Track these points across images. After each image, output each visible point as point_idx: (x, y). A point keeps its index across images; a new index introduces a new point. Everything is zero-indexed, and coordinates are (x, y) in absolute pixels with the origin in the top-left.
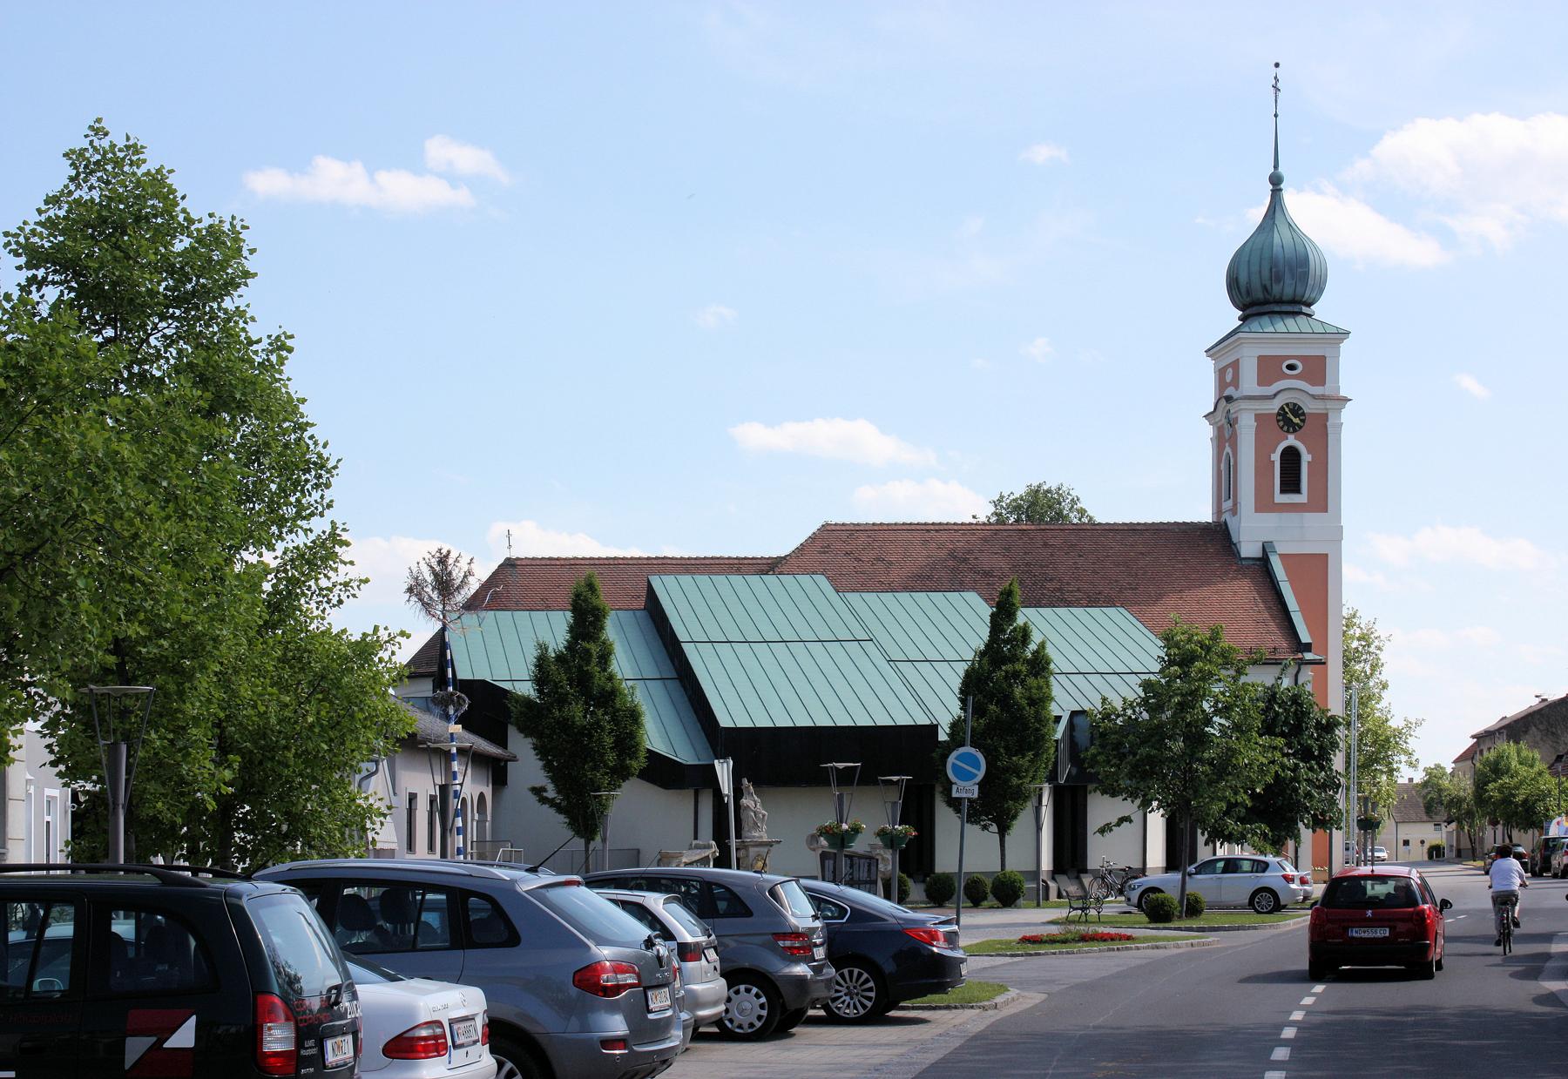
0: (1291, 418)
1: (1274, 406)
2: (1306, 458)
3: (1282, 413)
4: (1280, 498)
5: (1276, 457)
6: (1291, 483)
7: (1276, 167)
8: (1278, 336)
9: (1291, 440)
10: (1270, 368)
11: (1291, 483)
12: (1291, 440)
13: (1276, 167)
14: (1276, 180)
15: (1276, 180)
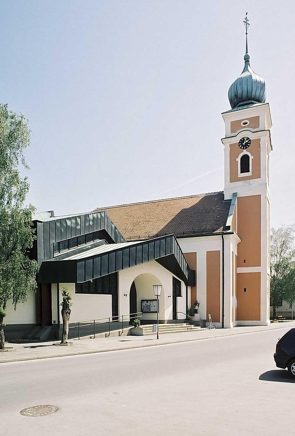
0: (244, 144)
1: (237, 140)
2: (251, 158)
3: (242, 141)
4: (241, 175)
5: (239, 160)
6: (245, 168)
8: (245, 114)
9: (245, 152)
10: (235, 126)
11: (245, 168)
12: (245, 152)
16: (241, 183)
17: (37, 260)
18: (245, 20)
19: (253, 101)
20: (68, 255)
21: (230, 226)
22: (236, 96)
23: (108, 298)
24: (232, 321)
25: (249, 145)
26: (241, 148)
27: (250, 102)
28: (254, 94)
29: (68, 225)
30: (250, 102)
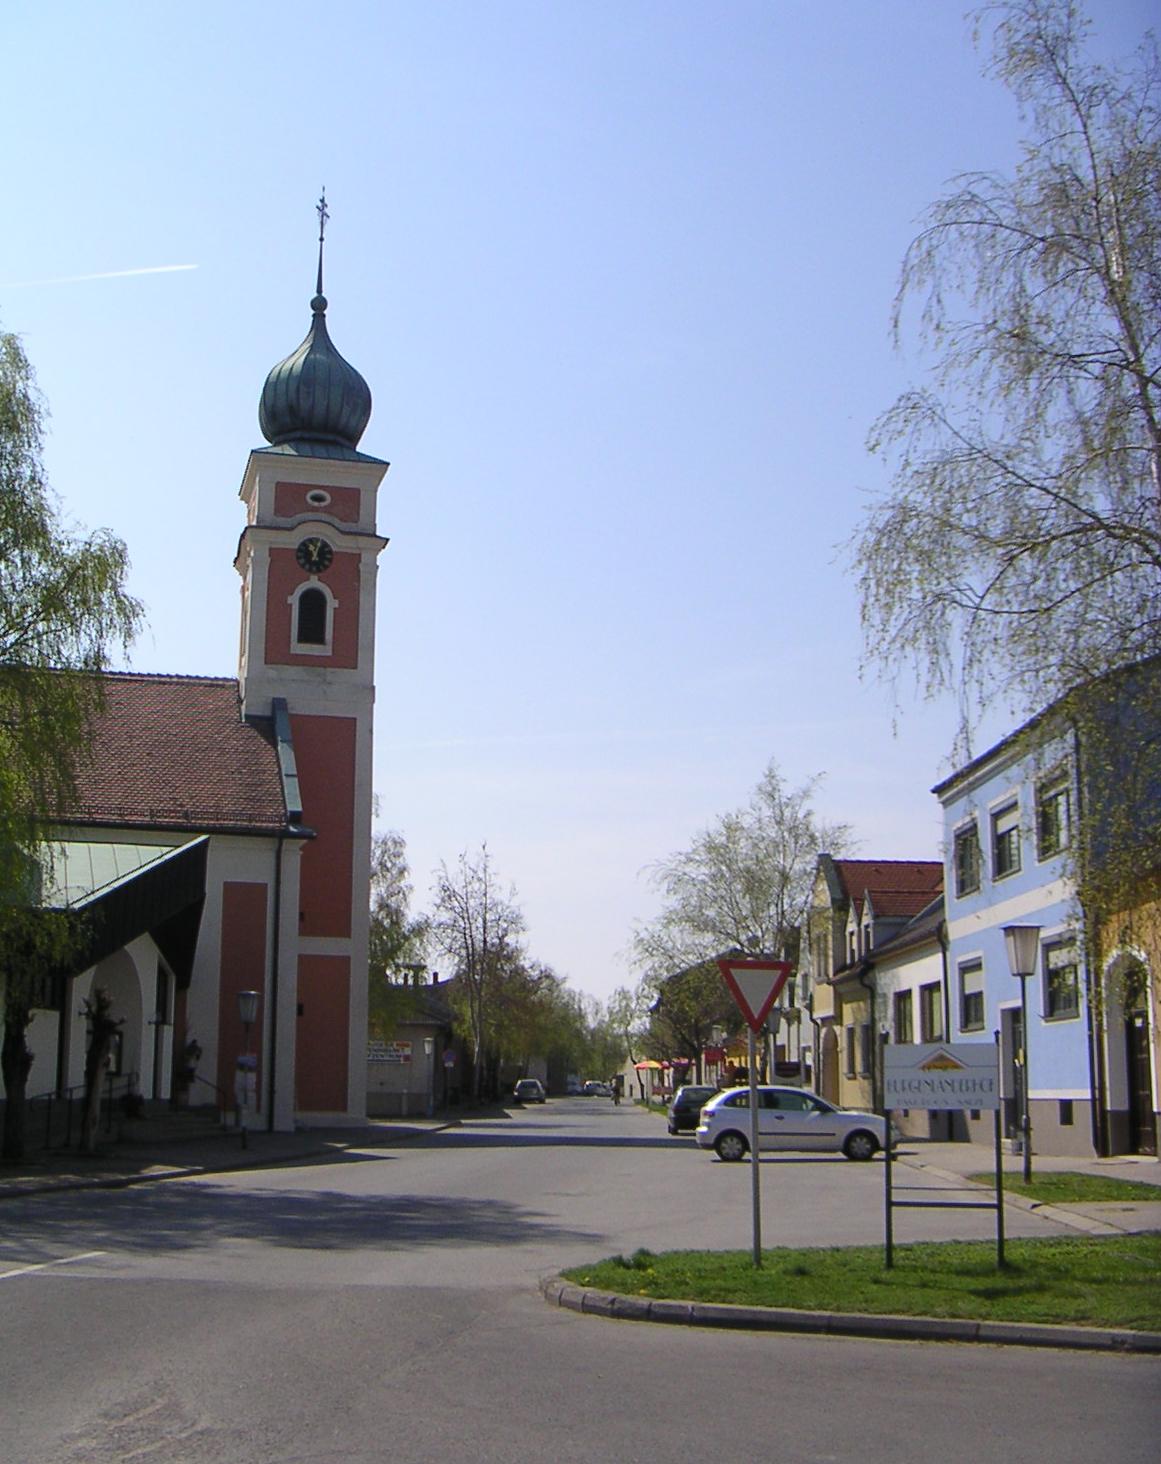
2: (332, 604)
3: (304, 550)
4: (299, 648)
5: (294, 600)
6: (311, 630)
7: (319, 290)
9: (314, 582)
11: (311, 630)
12: (314, 582)
13: (319, 290)
14: (319, 305)
15: (319, 305)
16: (292, 672)
17: (841, 1025)
18: (320, 204)
19: (340, 439)
20: (42, 1270)
21: (344, 1108)
22: (292, 410)
23: (925, 1135)
24: (958, 1026)
25: (307, 566)
27: (331, 437)
28: (343, 420)
29: (293, 1130)
30: (331, 437)
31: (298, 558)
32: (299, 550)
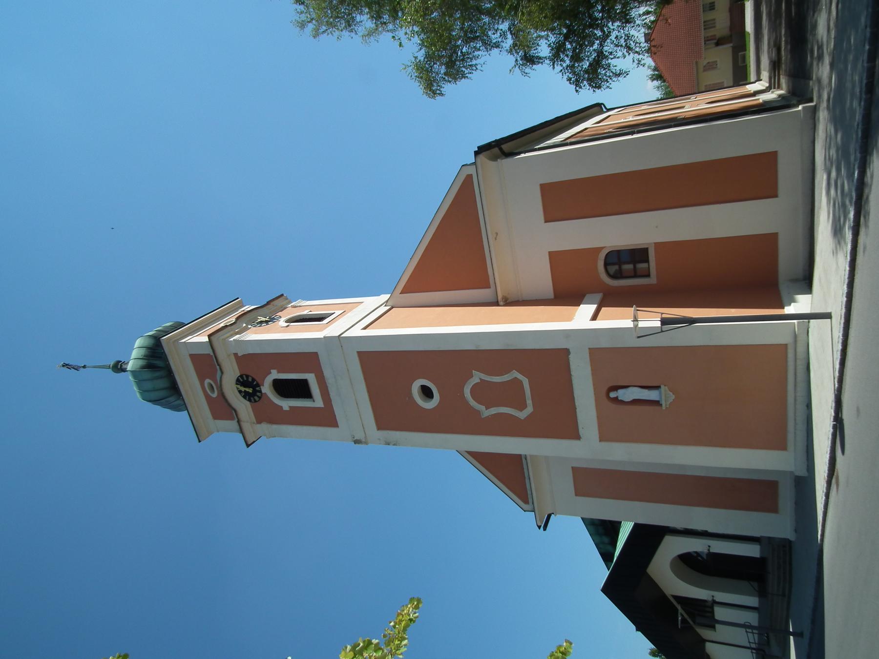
0: (249, 386)
2: (275, 375)
3: (246, 396)
5: (286, 404)
6: (300, 389)
9: (267, 388)
11: (300, 389)
26: (260, 398)
31: (255, 401)
32: (250, 400)
